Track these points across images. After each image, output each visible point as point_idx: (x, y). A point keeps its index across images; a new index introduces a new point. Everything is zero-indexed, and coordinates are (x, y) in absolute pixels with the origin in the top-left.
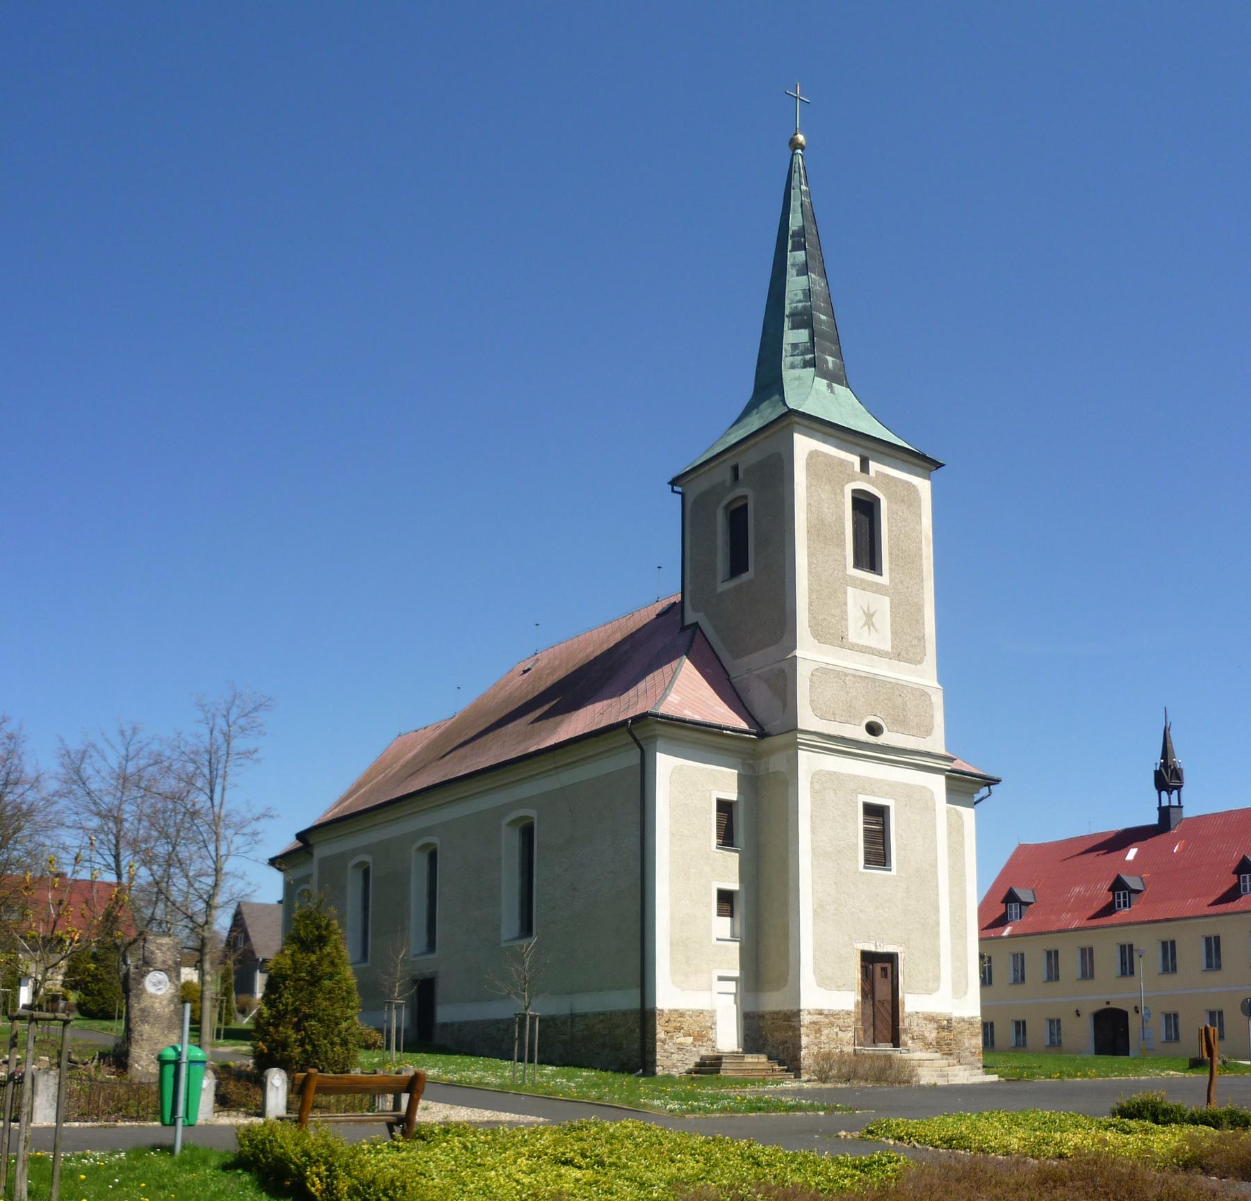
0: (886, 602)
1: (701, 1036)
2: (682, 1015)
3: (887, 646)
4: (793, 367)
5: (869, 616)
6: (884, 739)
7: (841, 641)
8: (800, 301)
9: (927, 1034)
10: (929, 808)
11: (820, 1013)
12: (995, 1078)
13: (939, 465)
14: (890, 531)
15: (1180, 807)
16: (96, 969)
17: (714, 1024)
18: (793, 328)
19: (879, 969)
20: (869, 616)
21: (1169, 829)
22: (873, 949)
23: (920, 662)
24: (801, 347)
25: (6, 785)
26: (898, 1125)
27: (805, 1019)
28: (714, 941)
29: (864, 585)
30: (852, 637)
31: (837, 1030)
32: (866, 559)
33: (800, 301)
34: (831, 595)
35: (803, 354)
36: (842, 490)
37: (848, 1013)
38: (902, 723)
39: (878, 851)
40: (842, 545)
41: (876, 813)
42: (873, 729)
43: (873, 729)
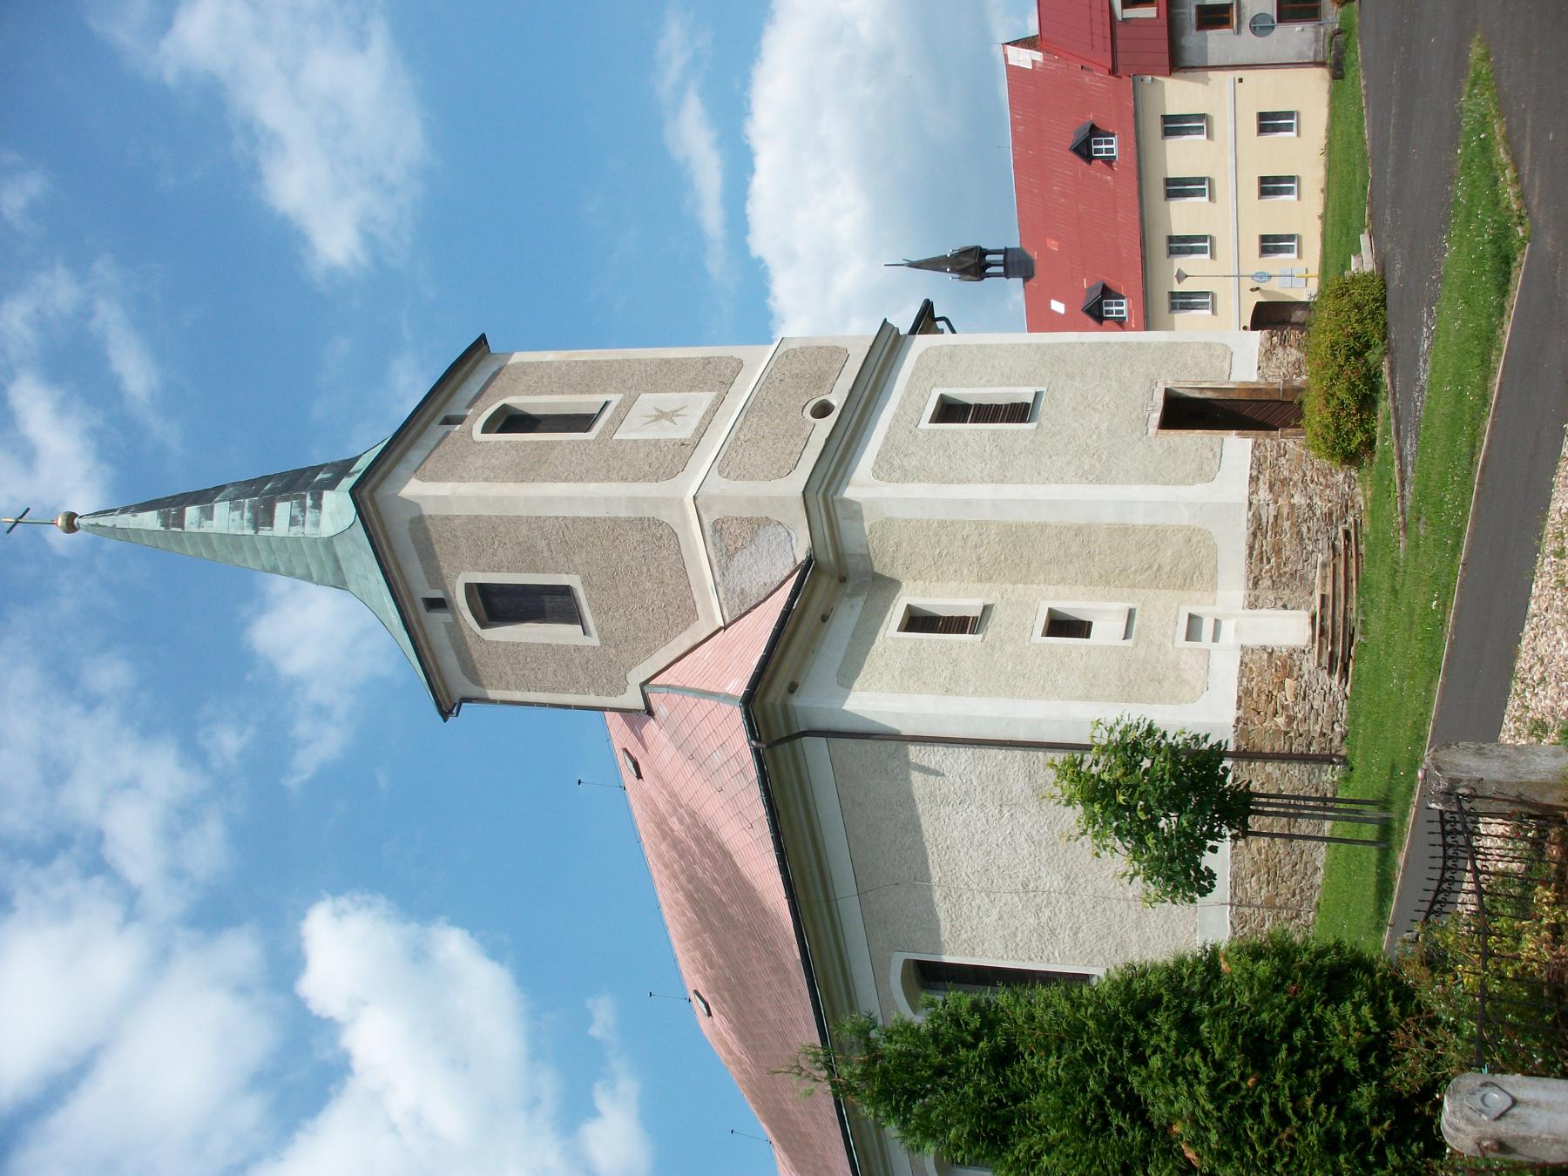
0: (646, 398)
1: (1284, 664)
2: (1247, 692)
4: (317, 524)
5: (661, 415)
6: (837, 400)
8: (242, 516)
9: (1292, 359)
10: (952, 353)
11: (1254, 480)
12: (1364, 240)
13: (482, 341)
15: (1005, 252)
16: (1546, 884)
17: (1264, 648)
18: (271, 525)
20: (661, 415)
21: (1032, 261)
24: (296, 512)
28: (1129, 643)
31: (1283, 461)
33: (242, 516)
35: (303, 510)
36: (479, 443)
37: (1256, 446)
38: (821, 380)
40: (552, 445)
41: (950, 411)
42: (823, 410)
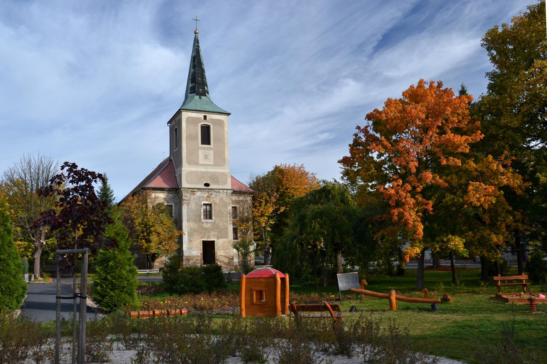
3: (212, 163)
7: (197, 164)
14: (213, 133)
19: (209, 248)
22: (206, 240)
23: (224, 166)
25: (471, 363)
26: (178, 355)
27: (184, 258)
29: (204, 149)
30: (200, 162)
32: (208, 217)
34: (193, 153)
37: (198, 256)
38: (217, 182)
39: (206, 139)
43: (207, 185)
